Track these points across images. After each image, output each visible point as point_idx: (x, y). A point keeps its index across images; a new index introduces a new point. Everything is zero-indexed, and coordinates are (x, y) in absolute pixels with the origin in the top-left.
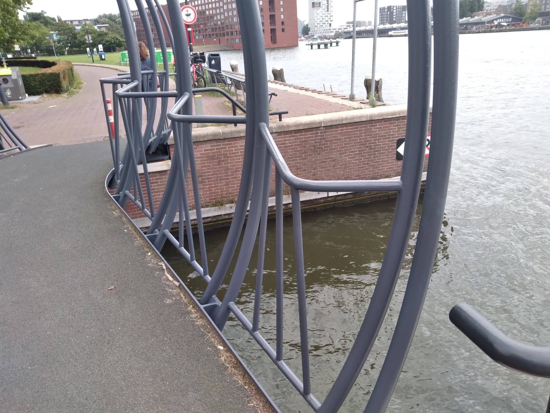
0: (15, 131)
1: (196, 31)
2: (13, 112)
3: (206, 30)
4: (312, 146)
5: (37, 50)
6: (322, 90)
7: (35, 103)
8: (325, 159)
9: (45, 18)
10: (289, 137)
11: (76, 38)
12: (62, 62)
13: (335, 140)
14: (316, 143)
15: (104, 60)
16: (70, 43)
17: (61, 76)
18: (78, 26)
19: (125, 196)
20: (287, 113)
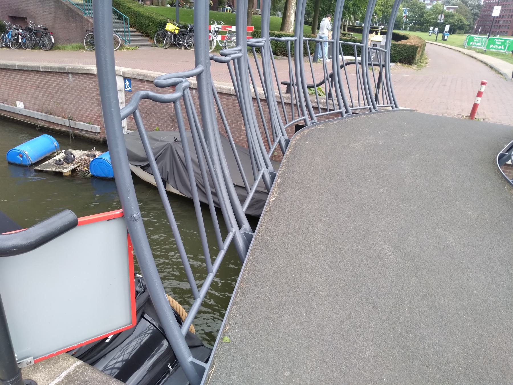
6: (374, 67)
11: (422, 16)
12: (414, 37)
15: (446, 40)
16: (415, 21)
18: (428, 5)
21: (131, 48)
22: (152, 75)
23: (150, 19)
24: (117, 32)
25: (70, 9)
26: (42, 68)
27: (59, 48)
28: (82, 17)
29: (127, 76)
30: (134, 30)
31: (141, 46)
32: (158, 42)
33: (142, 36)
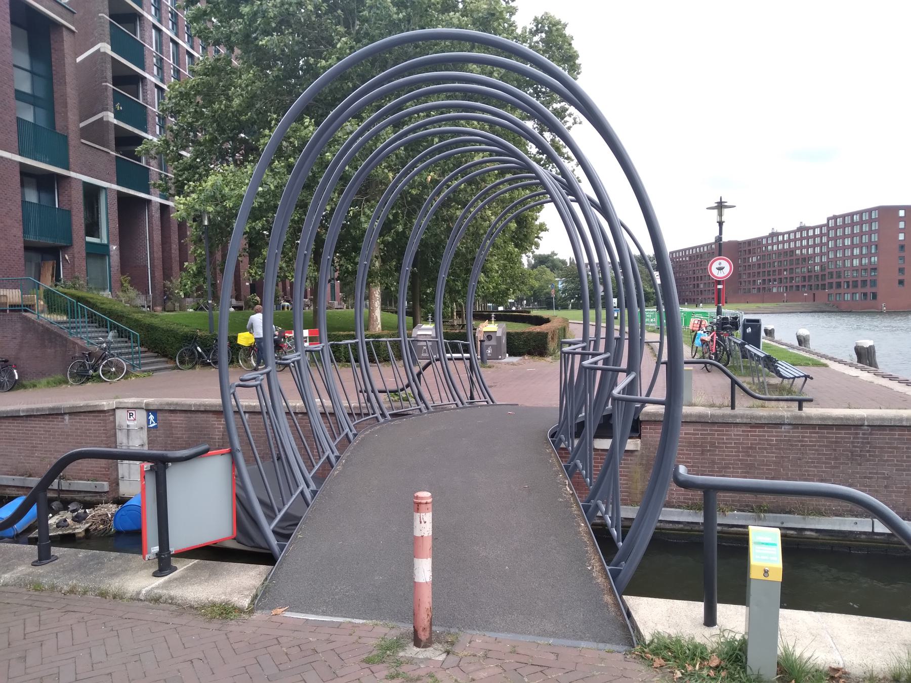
0: (489, 389)
1: (775, 280)
2: (489, 371)
3: (792, 279)
4: (847, 451)
5: (535, 301)
7: (513, 364)
8: (870, 473)
9: (553, 261)
10: (811, 433)
13: (889, 448)
14: (854, 447)
17: (549, 337)
19: (576, 466)
20: (811, 400)
21: (142, 375)
22: (188, 402)
23: (170, 332)
24: (121, 354)
25: (48, 329)
26: (23, 411)
27: (24, 387)
28: (66, 339)
29: (151, 408)
30: (143, 349)
31: (156, 370)
32: (182, 362)
33: (156, 357)
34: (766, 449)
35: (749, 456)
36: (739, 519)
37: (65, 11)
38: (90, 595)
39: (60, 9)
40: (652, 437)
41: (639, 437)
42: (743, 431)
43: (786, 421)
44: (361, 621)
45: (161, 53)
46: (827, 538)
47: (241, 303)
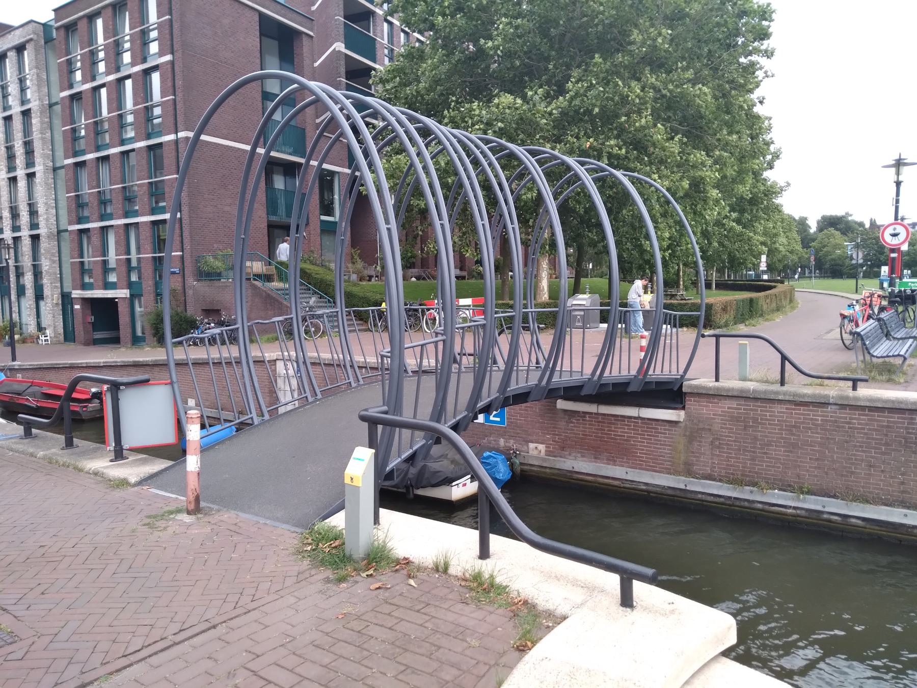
4: (901, 437)
9: (848, 222)
10: (859, 415)
14: (909, 433)
25: (269, 295)
28: (281, 303)
34: (810, 429)
35: (793, 434)
36: (778, 498)
37: (305, 20)
38: (71, 468)
39: (300, 18)
40: (696, 409)
41: (683, 408)
42: (787, 409)
43: (831, 401)
44: (174, 496)
45: (392, 44)
46: (877, 528)
47: (464, 273)
